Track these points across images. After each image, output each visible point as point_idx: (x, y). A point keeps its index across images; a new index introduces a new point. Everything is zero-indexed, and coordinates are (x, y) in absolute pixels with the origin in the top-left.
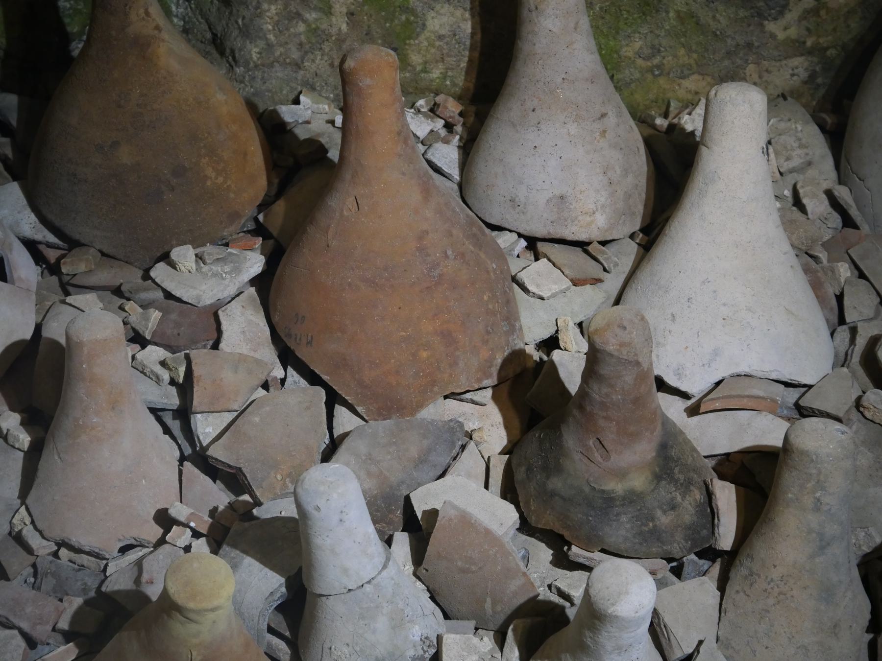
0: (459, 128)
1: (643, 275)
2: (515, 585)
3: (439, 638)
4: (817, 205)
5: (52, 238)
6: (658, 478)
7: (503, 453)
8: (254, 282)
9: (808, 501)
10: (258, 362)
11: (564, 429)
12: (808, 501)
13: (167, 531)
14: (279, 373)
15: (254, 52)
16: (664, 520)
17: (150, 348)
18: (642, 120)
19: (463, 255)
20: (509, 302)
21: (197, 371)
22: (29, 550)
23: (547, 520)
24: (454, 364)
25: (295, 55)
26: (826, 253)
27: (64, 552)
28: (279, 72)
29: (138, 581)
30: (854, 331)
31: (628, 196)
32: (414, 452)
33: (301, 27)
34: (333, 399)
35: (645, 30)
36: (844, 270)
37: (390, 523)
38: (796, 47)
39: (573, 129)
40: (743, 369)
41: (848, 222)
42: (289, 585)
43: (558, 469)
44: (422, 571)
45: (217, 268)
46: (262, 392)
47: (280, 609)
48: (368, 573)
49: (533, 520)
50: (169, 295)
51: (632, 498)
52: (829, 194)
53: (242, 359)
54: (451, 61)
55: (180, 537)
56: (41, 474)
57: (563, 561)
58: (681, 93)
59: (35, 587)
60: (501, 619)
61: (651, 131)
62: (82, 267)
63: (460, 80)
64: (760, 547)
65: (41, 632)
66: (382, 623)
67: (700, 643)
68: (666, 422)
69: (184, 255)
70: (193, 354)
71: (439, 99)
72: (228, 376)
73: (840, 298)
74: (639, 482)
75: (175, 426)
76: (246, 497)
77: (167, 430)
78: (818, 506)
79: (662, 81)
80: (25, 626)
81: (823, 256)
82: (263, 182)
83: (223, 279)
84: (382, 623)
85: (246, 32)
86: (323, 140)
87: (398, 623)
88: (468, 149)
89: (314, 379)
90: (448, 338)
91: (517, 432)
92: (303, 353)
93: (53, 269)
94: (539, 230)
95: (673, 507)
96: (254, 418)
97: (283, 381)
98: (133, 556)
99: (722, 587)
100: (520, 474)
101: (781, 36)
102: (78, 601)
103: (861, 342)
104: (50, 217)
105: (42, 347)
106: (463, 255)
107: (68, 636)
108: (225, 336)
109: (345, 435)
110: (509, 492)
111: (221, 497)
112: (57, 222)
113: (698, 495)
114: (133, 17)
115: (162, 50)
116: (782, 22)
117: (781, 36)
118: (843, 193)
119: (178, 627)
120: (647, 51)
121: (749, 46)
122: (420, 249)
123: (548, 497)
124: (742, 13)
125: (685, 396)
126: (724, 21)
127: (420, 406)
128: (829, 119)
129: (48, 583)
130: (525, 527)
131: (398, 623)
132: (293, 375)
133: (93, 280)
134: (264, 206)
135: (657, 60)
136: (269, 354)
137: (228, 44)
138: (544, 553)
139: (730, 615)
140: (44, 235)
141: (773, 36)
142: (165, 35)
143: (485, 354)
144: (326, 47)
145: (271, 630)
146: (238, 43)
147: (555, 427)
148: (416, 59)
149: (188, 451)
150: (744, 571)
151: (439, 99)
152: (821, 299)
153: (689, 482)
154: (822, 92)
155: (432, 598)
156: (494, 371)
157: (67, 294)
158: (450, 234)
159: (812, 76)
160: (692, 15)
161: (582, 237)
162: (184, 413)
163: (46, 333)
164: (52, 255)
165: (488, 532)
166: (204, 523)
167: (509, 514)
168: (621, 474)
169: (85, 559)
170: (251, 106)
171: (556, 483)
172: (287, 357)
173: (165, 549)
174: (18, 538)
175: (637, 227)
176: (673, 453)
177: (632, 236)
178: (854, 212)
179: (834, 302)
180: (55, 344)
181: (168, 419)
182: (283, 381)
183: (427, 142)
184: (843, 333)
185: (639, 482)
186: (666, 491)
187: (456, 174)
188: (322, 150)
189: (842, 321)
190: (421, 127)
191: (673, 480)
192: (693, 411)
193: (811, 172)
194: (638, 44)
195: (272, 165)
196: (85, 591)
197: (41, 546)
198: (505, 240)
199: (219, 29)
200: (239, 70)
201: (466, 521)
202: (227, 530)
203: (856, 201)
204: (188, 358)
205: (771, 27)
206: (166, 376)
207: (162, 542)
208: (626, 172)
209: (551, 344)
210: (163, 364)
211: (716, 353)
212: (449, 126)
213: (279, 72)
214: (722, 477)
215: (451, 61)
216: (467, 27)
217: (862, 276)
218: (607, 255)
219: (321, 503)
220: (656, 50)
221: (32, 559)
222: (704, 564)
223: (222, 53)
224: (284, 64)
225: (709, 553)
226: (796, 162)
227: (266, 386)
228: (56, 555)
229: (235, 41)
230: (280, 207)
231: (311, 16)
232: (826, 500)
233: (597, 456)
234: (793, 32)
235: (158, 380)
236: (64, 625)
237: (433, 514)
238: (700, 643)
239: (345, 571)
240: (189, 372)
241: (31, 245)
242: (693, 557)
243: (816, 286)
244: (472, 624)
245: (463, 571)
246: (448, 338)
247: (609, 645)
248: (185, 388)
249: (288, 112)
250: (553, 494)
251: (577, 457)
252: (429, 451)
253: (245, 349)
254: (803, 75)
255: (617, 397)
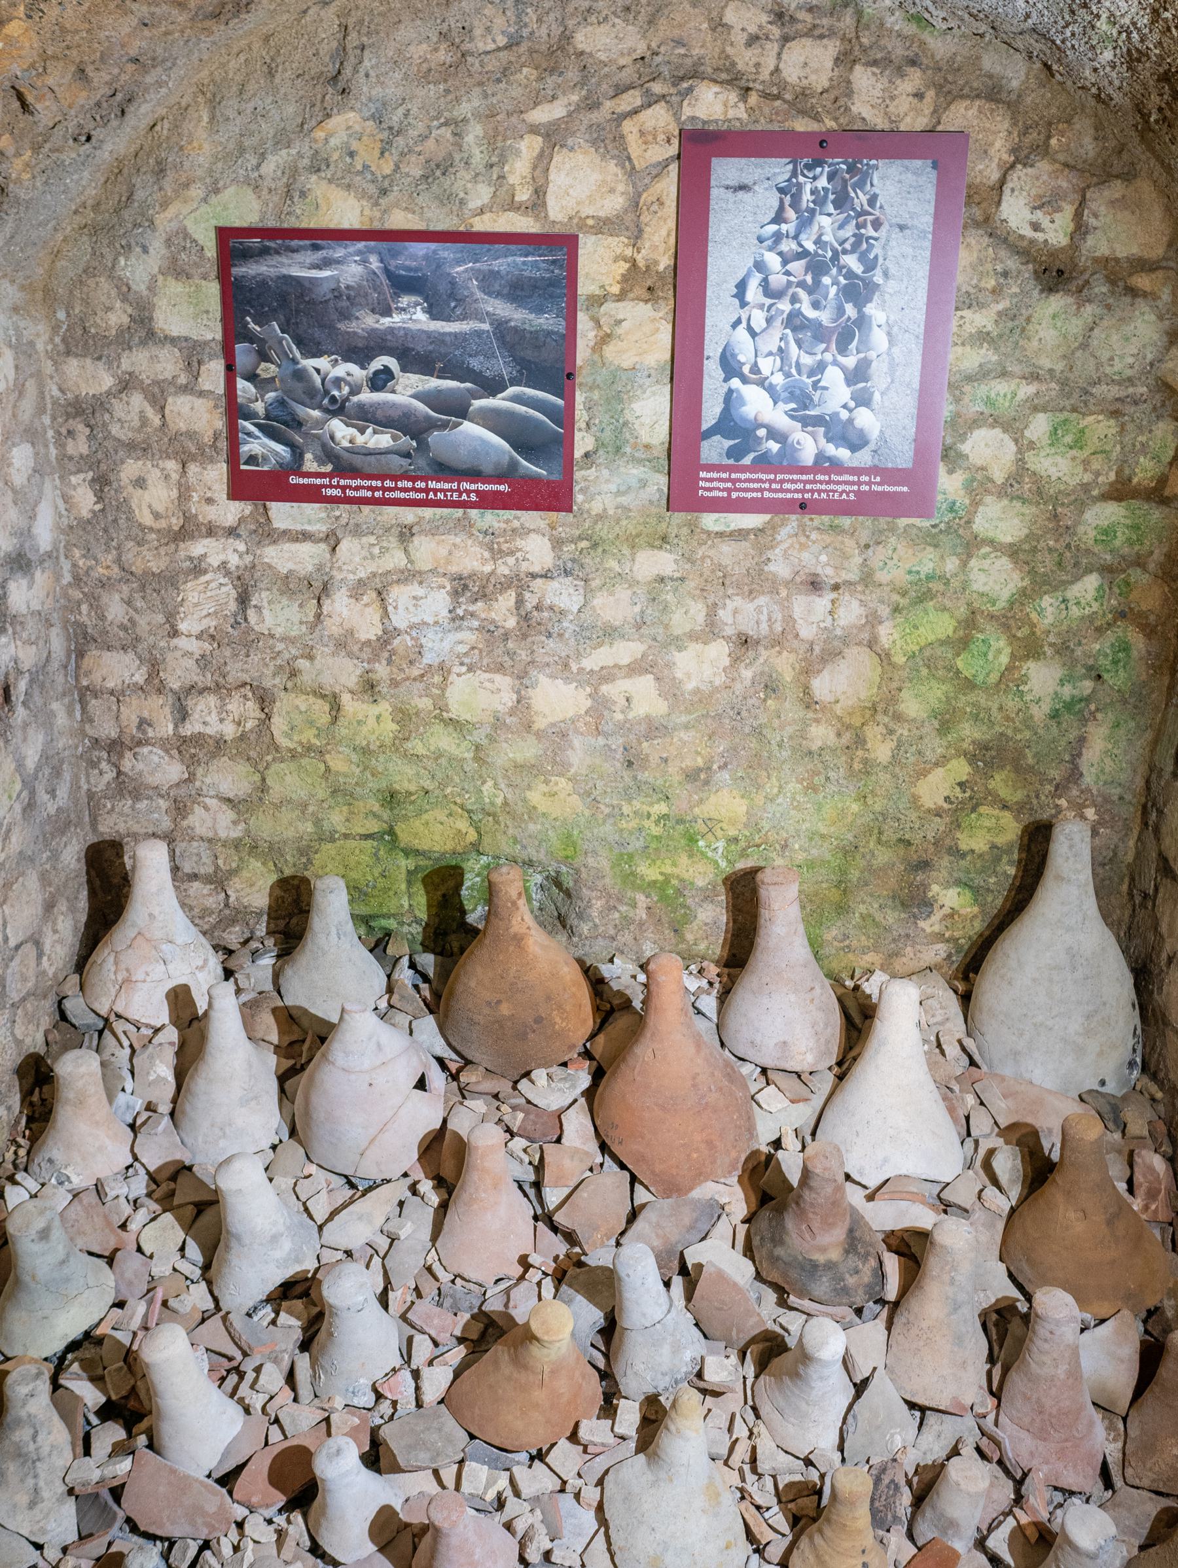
0: (717, 985)
1: (837, 1100)
2: (752, 1321)
3: (702, 1358)
4: (952, 1050)
5: (454, 1057)
6: (847, 1252)
7: (743, 1222)
8: (584, 1094)
9: (946, 1278)
10: (587, 1153)
11: (786, 1215)
12: (946, 1278)
13: (526, 1271)
14: (599, 1159)
15: (585, 928)
16: (851, 1281)
17: (516, 1139)
18: (837, 981)
19: (721, 1089)
20: (750, 1118)
21: (547, 1159)
22: (437, 1279)
23: (774, 1276)
24: (713, 1162)
25: (612, 932)
26: (933, 175)
27: (458, 1280)
28: (601, 942)
29: (506, 1305)
30: (977, 1142)
31: (828, 1042)
32: (687, 1221)
33: (617, 915)
34: (634, 1179)
35: (839, 924)
36: (971, 1100)
37: (670, 1269)
38: (939, 937)
39: (793, 998)
40: (903, 1172)
41: (973, 1063)
42: (606, 1318)
43: (781, 1242)
44: (691, 1306)
45: (561, 1085)
46: (589, 1174)
47: (600, 1332)
48: (658, 1318)
49: (764, 1274)
50: (529, 1102)
51: (830, 1266)
52: (960, 1042)
53: (576, 1151)
54: (712, 939)
55: (534, 1276)
56: (446, 1228)
57: (782, 1303)
58: (863, 964)
59: (439, 1304)
60: (742, 1343)
61: (843, 990)
62: (473, 1079)
63: (718, 951)
64: (914, 1303)
65: (443, 1338)
66: (666, 1350)
67: (875, 1369)
68: (853, 1211)
69: (540, 1075)
70: (545, 1146)
71: (705, 964)
72: (567, 1163)
73: (967, 1118)
74: (835, 1255)
75: (531, 1192)
76: (577, 1250)
77: (526, 1195)
78: (952, 1282)
79: (850, 955)
80: (434, 1334)
81: (956, 1088)
82: (590, 1022)
83: (608, 1409)
84: (666, 1350)
85: (580, 916)
86: (628, 992)
87: (677, 1349)
88: (725, 996)
89: (623, 1166)
90: (710, 1144)
91: (754, 1207)
92: (615, 1148)
93: (455, 1077)
94: (768, 1063)
95: (857, 1272)
96: (583, 1193)
97: (602, 1165)
98: (503, 1285)
99: (889, 1328)
100: (756, 1241)
101: (928, 930)
102: (467, 1316)
103: (982, 1152)
104: (454, 1043)
105: (447, 1136)
106: (721, 1089)
107: (461, 1340)
108: (566, 1133)
109: (643, 1206)
110: (749, 1251)
111: (561, 1247)
112: (459, 1048)
113: (873, 1263)
114: (514, 922)
115: (531, 941)
116: (929, 922)
117: (928, 930)
118: (969, 1043)
119: (535, 1349)
120: (840, 937)
121: (908, 936)
122: (694, 1086)
123: (774, 1260)
124: (903, 915)
125: (865, 1187)
126: (891, 921)
127: (691, 1189)
128: (961, 987)
129: (448, 1302)
130: (758, 1277)
131: (677, 1349)
132: (608, 1162)
133: (480, 1088)
134: (592, 1037)
135: (847, 942)
136: (593, 1146)
137: (569, 922)
138: (771, 1296)
139: (894, 1349)
140: (447, 1054)
141: (923, 930)
142: (533, 932)
143: (734, 1154)
144: (632, 927)
145: (592, 1345)
146: (575, 922)
147: (780, 1210)
148: (690, 937)
149: (539, 1212)
150: (904, 1320)
151: (705, 964)
152: (955, 1120)
153: (868, 1254)
154: (955, 966)
155: (697, 1325)
156: (740, 1166)
157: (464, 1097)
158: (713, 1074)
159: (949, 956)
160: (870, 916)
161: (797, 1069)
162: (537, 1185)
163: (451, 1126)
164: (453, 1067)
165: (735, 1284)
166: (550, 1267)
167: (749, 1268)
168: (823, 1250)
169: (471, 1286)
170: (580, 962)
171: (779, 1251)
172: (604, 1147)
173: (524, 1284)
174: (429, 1269)
175: (834, 1062)
176: (857, 1234)
177: (830, 1069)
178: (977, 1057)
179: (964, 1121)
180: (457, 1137)
181: (527, 1188)
182: (602, 1165)
183: (697, 994)
184: (969, 1143)
185: (835, 1255)
186: (853, 1262)
187: (714, 1017)
188: (628, 1002)
189: (969, 1134)
190: (693, 984)
191: (857, 1253)
192: (870, 1198)
193: (948, 1025)
194: (834, 932)
195: (597, 1009)
196: (471, 1308)
197: (444, 1277)
198: (746, 1069)
199: (563, 912)
200: (575, 939)
201: (721, 1276)
202: (565, 1272)
203: (978, 1048)
204: (541, 1148)
205: (921, 924)
206: (526, 1159)
207: (522, 1278)
208: (826, 1025)
209: (777, 1144)
210: (525, 1150)
211: (886, 1160)
212: (711, 984)
213: (601, 942)
214: (890, 1249)
215: (712, 939)
216: (724, 919)
217: (982, 1103)
218: (814, 1082)
219: (631, 1272)
220: (846, 937)
221: (437, 1285)
222: (878, 1308)
223: (564, 927)
224: (604, 937)
225: (881, 1301)
226: (939, 1018)
227: (591, 1170)
228: (453, 1282)
229: (573, 920)
230: (601, 1039)
231: (623, 908)
232: (958, 1278)
233: (807, 1236)
234: (936, 928)
235: (521, 1162)
236: (458, 1333)
237: (699, 1267)
238: (875, 1369)
239: (644, 1315)
240: (542, 1159)
241: (441, 1061)
242: (871, 1303)
243: (951, 1110)
244: (723, 1344)
245: (720, 1309)
246: (710, 1144)
247: (815, 1376)
248: (539, 1168)
249: (606, 970)
250: (778, 1258)
251: (794, 1236)
252: (696, 1220)
253: (577, 1144)
254: (944, 955)
255: (821, 1201)
